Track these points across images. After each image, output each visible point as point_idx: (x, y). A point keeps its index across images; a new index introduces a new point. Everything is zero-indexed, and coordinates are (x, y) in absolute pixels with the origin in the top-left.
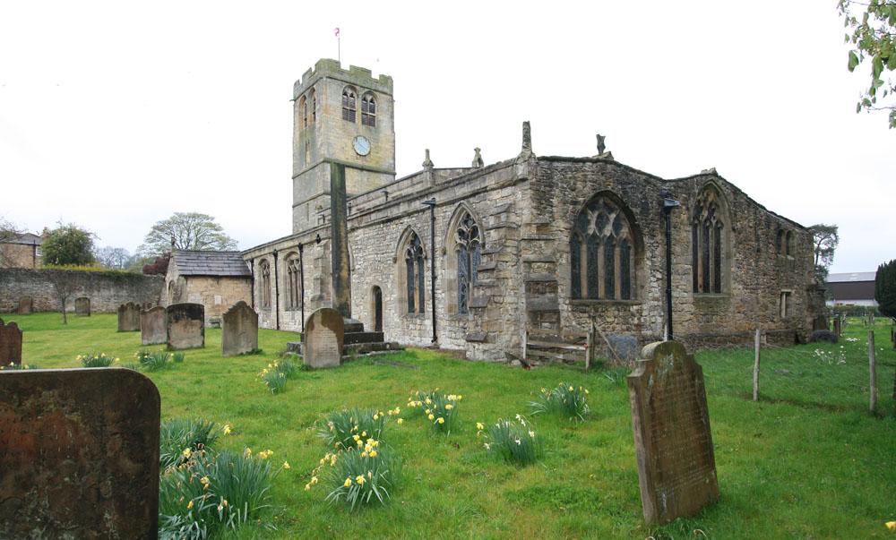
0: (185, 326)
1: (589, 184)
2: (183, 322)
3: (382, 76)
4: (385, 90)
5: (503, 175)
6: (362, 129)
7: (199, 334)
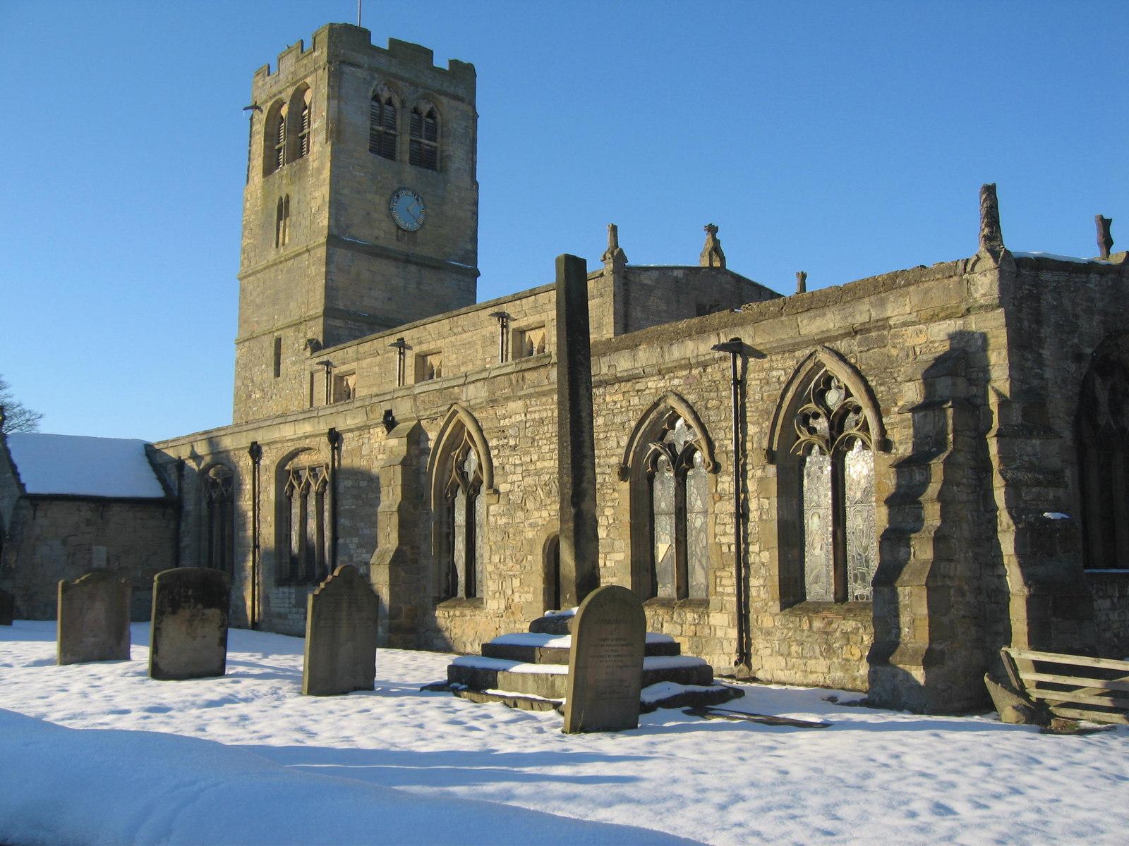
0: (190, 622)
1: (1097, 318)
2: (185, 613)
3: (454, 63)
4: (461, 92)
5: (934, 293)
6: (410, 173)
7: (217, 641)
